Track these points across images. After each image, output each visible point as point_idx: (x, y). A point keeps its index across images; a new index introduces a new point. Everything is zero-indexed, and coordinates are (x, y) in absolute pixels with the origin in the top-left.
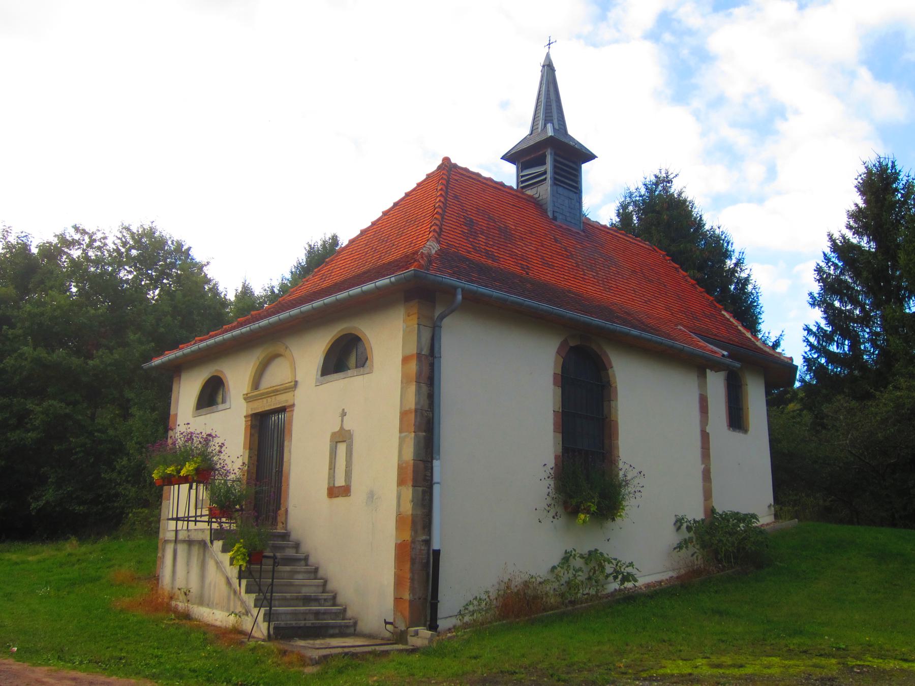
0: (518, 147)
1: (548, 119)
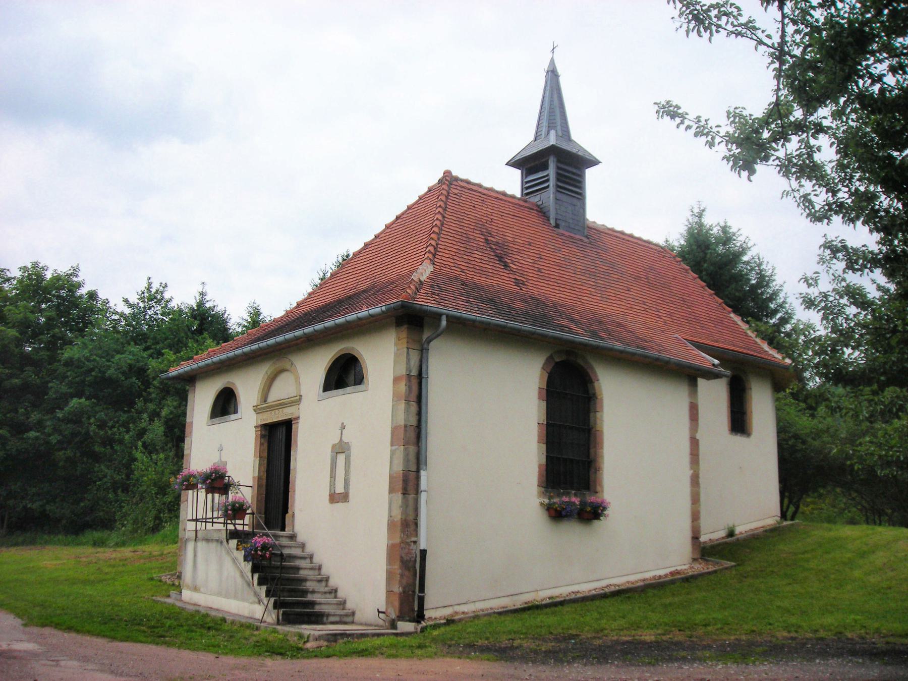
0: (519, 155)
1: (551, 126)
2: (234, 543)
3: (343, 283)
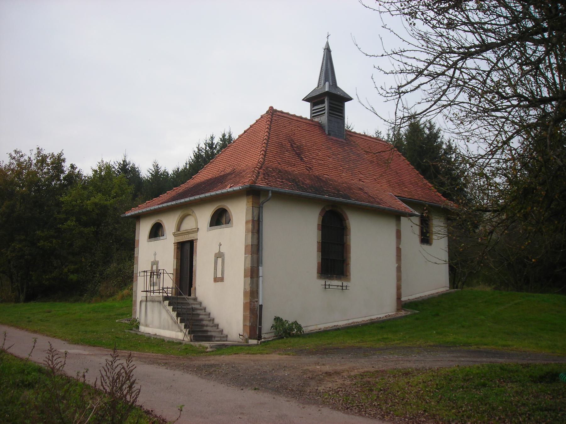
0: (309, 95)
1: (326, 80)
2: (167, 302)
3: (217, 167)
